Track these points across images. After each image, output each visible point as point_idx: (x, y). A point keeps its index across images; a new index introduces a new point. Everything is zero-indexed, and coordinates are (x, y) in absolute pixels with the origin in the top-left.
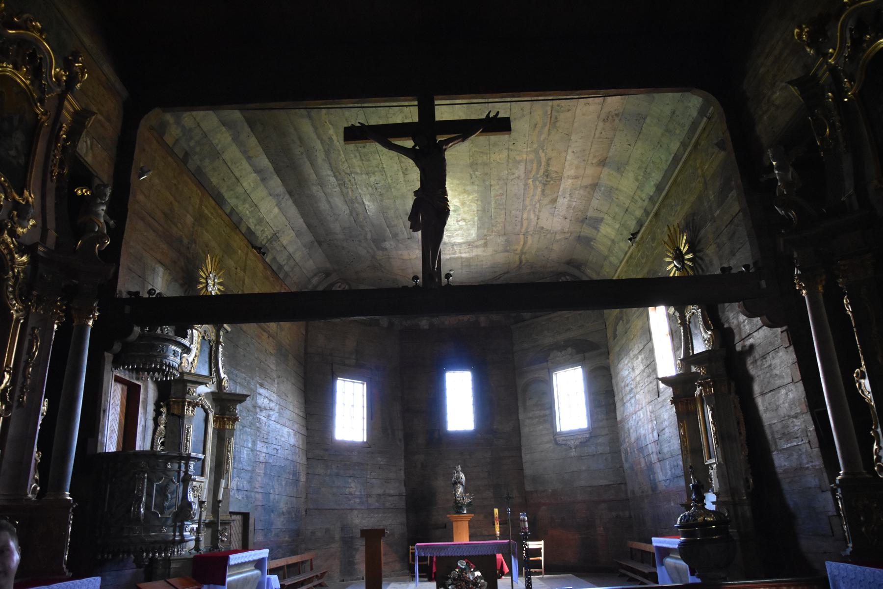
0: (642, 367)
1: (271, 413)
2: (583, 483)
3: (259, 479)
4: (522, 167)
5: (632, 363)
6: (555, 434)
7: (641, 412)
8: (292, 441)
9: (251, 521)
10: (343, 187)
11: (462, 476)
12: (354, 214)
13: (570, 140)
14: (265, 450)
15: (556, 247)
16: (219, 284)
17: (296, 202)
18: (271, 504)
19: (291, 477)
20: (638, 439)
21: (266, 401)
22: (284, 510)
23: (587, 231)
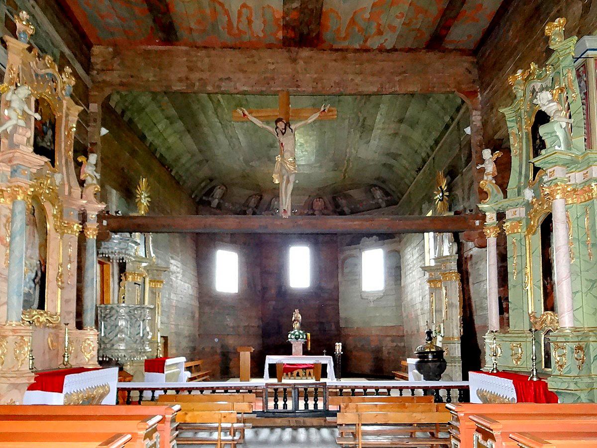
0: (417, 255)
1: (178, 275)
2: (377, 324)
3: (173, 316)
4: (347, 121)
5: (412, 251)
6: (361, 292)
7: (414, 283)
8: (191, 292)
9: (169, 342)
10: (225, 129)
12: (232, 144)
13: (379, 107)
14: (175, 299)
16: (147, 197)
17: (192, 137)
19: (190, 314)
23: (392, 162)
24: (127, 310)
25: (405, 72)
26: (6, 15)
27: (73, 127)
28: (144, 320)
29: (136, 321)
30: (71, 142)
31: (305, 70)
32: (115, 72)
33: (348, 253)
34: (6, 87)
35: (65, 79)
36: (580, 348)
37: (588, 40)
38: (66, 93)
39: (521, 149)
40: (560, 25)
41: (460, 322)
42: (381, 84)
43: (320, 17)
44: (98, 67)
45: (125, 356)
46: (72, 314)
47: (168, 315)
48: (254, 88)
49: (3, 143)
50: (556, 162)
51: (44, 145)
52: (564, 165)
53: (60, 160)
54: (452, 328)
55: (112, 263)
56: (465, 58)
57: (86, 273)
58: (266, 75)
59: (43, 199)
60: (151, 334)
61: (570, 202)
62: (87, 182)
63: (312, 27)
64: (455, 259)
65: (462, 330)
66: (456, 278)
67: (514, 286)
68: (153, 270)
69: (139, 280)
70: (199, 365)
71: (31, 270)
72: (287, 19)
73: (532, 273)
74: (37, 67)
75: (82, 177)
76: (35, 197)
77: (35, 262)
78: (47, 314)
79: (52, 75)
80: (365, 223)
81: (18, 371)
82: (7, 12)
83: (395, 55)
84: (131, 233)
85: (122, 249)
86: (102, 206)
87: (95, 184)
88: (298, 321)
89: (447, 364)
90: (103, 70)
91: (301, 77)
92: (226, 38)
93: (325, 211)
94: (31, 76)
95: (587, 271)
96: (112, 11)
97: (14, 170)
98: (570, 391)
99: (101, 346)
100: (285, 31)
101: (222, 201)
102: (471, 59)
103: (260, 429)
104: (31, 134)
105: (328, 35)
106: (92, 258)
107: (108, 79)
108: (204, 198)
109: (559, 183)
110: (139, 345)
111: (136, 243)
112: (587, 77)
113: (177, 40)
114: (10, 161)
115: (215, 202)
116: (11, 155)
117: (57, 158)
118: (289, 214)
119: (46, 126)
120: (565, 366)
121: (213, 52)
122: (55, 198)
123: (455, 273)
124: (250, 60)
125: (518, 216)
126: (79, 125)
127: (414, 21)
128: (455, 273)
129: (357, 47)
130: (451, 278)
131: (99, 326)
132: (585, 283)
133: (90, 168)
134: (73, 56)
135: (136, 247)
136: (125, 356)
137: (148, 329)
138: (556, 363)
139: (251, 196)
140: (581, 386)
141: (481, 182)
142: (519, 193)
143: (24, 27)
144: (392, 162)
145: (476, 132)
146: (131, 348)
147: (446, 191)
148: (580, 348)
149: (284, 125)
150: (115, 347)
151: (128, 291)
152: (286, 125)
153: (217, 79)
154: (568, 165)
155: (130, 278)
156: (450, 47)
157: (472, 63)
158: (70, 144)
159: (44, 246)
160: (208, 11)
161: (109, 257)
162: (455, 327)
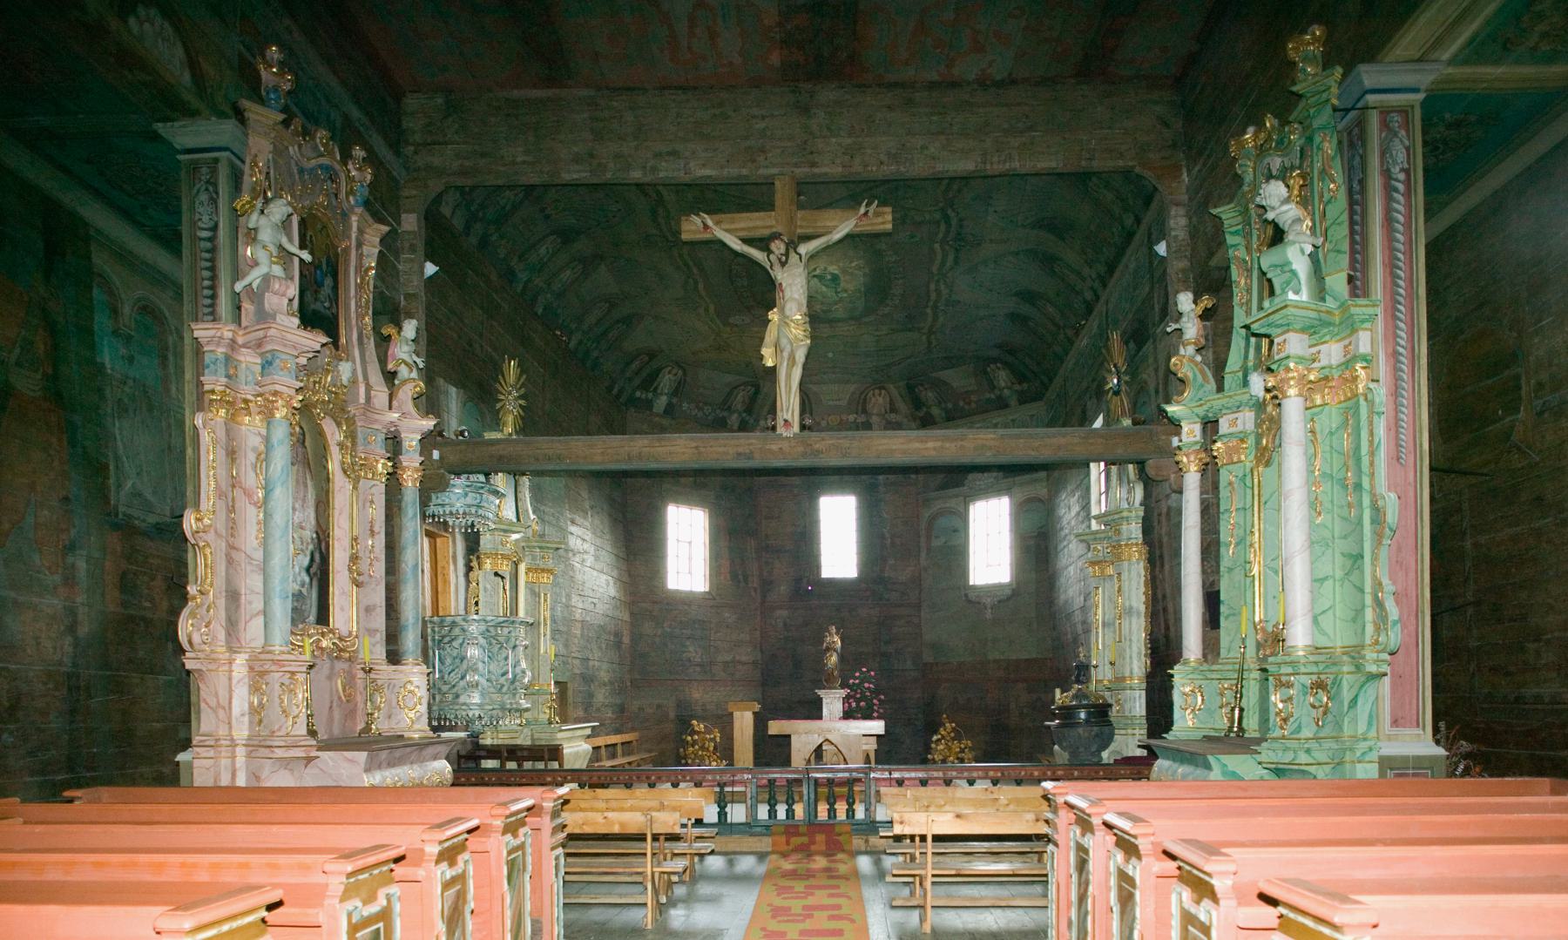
1: (585, 557)
2: (997, 655)
3: (576, 641)
8: (612, 591)
9: (570, 693)
11: (836, 638)
14: (580, 605)
15: (713, 868)
18: (591, 672)
19: (612, 638)
20: (1066, 602)
21: (579, 542)
22: (606, 680)
23: (1025, 309)
24: (483, 628)
25: (1031, 128)
26: (240, 55)
27: (371, 268)
28: (515, 647)
29: (500, 649)
30: (368, 296)
31: (829, 129)
32: (449, 147)
33: (938, 505)
34: (248, 202)
35: (353, 173)
36: (1319, 685)
37: (1367, 72)
38: (357, 201)
39: (1249, 291)
40: (1315, 39)
41: (1145, 645)
44: (417, 138)
45: (480, 717)
46: (378, 635)
47: (567, 640)
48: (725, 172)
49: (246, 310)
50: (1288, 325)
51: (317, 306)
52: (1303, 331)
54: (1131, 658)
55: (453, 534)
57: (403, 633)
59: (319, 414)
60: (529, 673)
61: (1319, 402)
62: (399, 375)
64: (1137, 517)
65: (1148, 662)
66: (1140, 555)
67: (1230, 570)
68: (534, 547)
69: (505, 569)
70: (631, 742)
71: (302, 550)
73: (1262, 543)
74: (301, 155)
75: (391, 366)
76: (305, 409)
77: (309, 534)
78: (334, 634)
79: (327, 168)
81: (287, 735)
84: (487, 475)
85: (469, 506)
86: (429, 423)
87: (414, 379)
88: (835, 650)
89: (1116, 732)
90: (426, 144)
93: (893, 416)
95: (1345, 537)
97: (267, 362)
98: (1296, 767)
99: (434, 698)
101: (675, 400)
103: (738, 857)
104: (293, 290)
106: (411, 524)
107: (436, 161)
108: (638, 394)
109: (1292, 365)
110: (507, 696)
111: (496, 493)
112: (1365, 151)
114: (259, 344)
115: (661, 403)
116: (261, 334)
117: (342, 331)
118: (796, 428)
119: (321, 269)
120: (1292, 720)
122: (339, 411)
123: (1137, 544)
124: (717, 112)
125: (1240, 428)
126: (381, 257)
128: (1137, 544)
129: (935, 77)
130: (1130, 556)
131: (431, 659)
132: (1339, 559)
133: (406, 348)
135: (497, 502)
136: (480, 717)
137: (524, 665)
138: (1277, 714)
139: (735, 388)
140: (1321, 756)
141: (1173, 360)
142: (1245, 383)
144: (1025, 309)
145: (1175, 252)
146: (492, 702)
147: (1126, 373)
148: (1319, 685)
150: (462, 699)
151: (485, 590)
152: (787, 245)
154: (1314, 329)
155: (488, 565)
158: (367, 301)
159: (323, 505)
161: (445, 523)
162: (1135, 655)
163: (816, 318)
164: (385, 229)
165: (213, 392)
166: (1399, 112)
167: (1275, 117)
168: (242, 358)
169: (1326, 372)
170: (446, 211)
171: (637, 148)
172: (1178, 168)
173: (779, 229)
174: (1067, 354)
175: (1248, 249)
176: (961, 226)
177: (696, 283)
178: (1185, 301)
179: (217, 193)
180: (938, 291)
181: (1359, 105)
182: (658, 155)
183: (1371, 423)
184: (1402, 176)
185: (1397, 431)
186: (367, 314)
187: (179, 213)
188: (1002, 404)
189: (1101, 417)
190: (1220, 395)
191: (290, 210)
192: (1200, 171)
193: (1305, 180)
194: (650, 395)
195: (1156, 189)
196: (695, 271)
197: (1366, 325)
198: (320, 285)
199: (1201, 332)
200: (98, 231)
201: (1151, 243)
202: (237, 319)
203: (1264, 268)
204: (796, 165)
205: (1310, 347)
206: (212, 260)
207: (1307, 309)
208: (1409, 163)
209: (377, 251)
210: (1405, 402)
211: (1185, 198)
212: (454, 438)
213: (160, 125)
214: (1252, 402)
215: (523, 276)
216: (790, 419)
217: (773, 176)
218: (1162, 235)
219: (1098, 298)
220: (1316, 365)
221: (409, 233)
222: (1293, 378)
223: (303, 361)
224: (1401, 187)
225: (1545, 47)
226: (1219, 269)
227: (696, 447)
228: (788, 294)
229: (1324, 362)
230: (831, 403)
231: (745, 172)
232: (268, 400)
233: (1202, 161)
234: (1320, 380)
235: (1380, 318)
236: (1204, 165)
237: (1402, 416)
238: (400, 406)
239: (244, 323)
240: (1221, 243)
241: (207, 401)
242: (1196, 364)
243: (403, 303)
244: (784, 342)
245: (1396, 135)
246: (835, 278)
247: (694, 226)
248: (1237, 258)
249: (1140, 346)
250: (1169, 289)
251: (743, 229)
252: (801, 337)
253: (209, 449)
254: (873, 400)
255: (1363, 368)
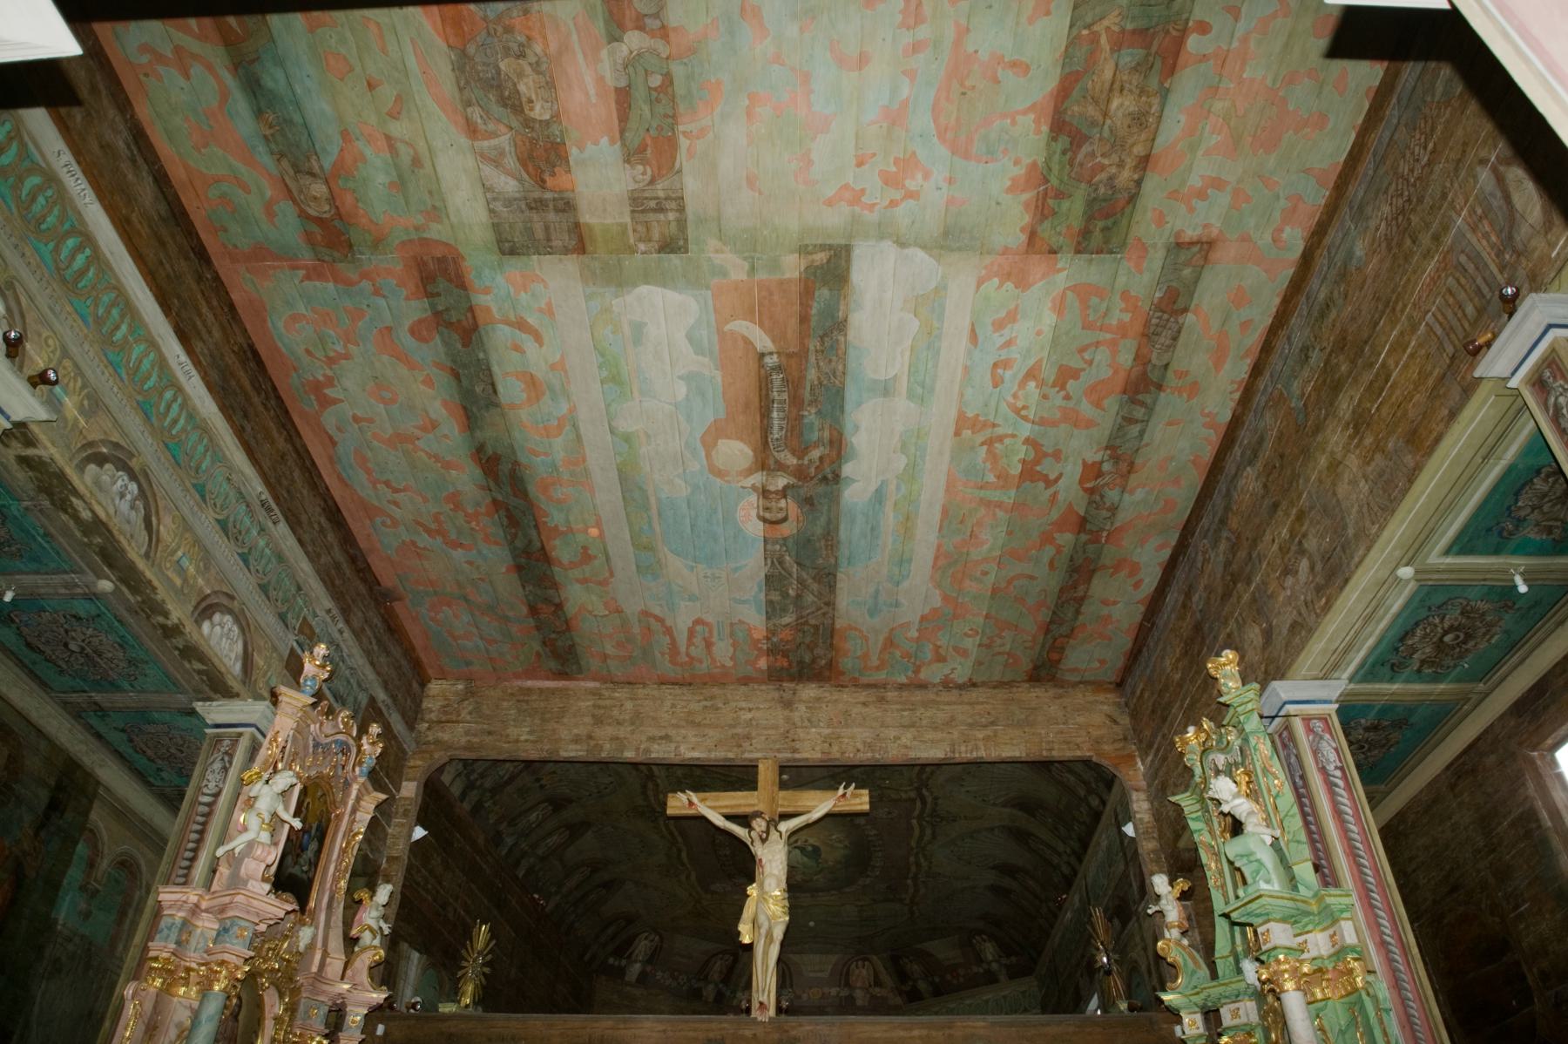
25: (993, 723)
26: (292, 650)
30: (350, 860)
31: (809, 720)
38: (361, 771)
42: (953, 745)
43: (832, 637)
44: (433, 716)
50: (1267, 914)
51: (296, 870)
52: (1284, 920)
53: (318, 898)
56: (1101, 697)
58: (735, 731)
62: (361, 942)
63: (819, 651)
72: (775, 639)
75: (354, 932)
80: (934, 1033)
82: (295, 644)
83: (974, 694)
87: (375, 947)
91: (801, 733)
92: (666, 667)
94: (306, 747)
96: (474, 630)
100: (771, 658)
101: (649, 968)
102: (1112, 697)
104: (274, 855)
105: (847, 663)
108: (611, 960)
112: (1297, 749)
113: (580, 671)
114: (223, 909)
116: (227, 899)
117: (314, 895)
118: (772, 1012)
121: (641, 692)
124: (708, 703)
125: (1244, 1020)
126: (374, 821)
127: (999, 641)
129: (903, 679)
134: (389, 701)
141: (1160, 944)
142: (1239, 971)
143: (316, 669)
149: (764, 824)
153: (644, 738)
156: (1074, 678)
157: (1118, 705)
158: (346, 867)
160: (636, 630)
163: (795, 887)
164: (383, 797)
165: (156, 959)
166: (1320, 719)
167: (1211, 720)
168: (199, 923)
169: (1319, 963)
170: (446, 778)
171: (633, 732)
172: (1131, 757)
173: (760, 807)
174: (1052, 927)
175: (1211, 832)
176: (936, 804)
177: (680, 851)
178: (1160, 883)
179: (231, 763)
180: (918, 865)
181: (1281, 713)
182: (652, 739)
183: (1381, 1022)
184: (1338, 773)
185: (1412, 1028)
186: (344, 877)
187: (189, 777)
188: (991, 979)
189: (1095, 997)
190: (1214, 983)
191: (294, 781)
192: (1153, 761)
193: (1250, 777)
194: (624, 962)
195: (1115, 776)
196: (680, 839)
197: (1345, 915)
198: (303, 849)
199: (1183, 915)
200: (107, 789)
201: (1119, 826)
202: (208, 885)
203: (1231, 858)
204: (779, 751)
205: (1295, 936)
206: (204, 824)
207: (1282, 898)
208: (1340, 761)
209: (369, 817)
210: (1409, 995)
211: (1143, 784)
212: (404, 1010)
213: (200, 703)
214: (1250, 991)
215: (509, 841)
216: (766, 1002)
217: (757, 760)
218: (1129, 818)
219: (1075, 873)
220: (1305, 956)
221: (405, 799)
222: (1286, 971)
223: (263, 927)
224: (1341, 783)
225: (1427, 671)
226: (1189, 850)
227: (664, 1031)
228: (767, 869)
229: (1314, 953)
230: (811, 975)
231: (731, 755)
232: (211, 970)
233: (1153, 751)
234: (1315, 972)
235: (1358, 906)
236: (1156, 755)
237: (1412, 1011)
238: (353, 976)
239: (215, 887)
240: (1185, 827)
241: (146, 968)
242: (1183, 948)
243: (384, 865)
244: (762, 919)
245: (1321, 738)
246: (816, 850)
247: (680, 803)
248: (1201, 842)
249: (1124, 924)
250: (1144, 869)
251: (726, 807)
252: (779, 913)
253: (128, 1025)
254: (857, 972)
255: (1355, 960)
